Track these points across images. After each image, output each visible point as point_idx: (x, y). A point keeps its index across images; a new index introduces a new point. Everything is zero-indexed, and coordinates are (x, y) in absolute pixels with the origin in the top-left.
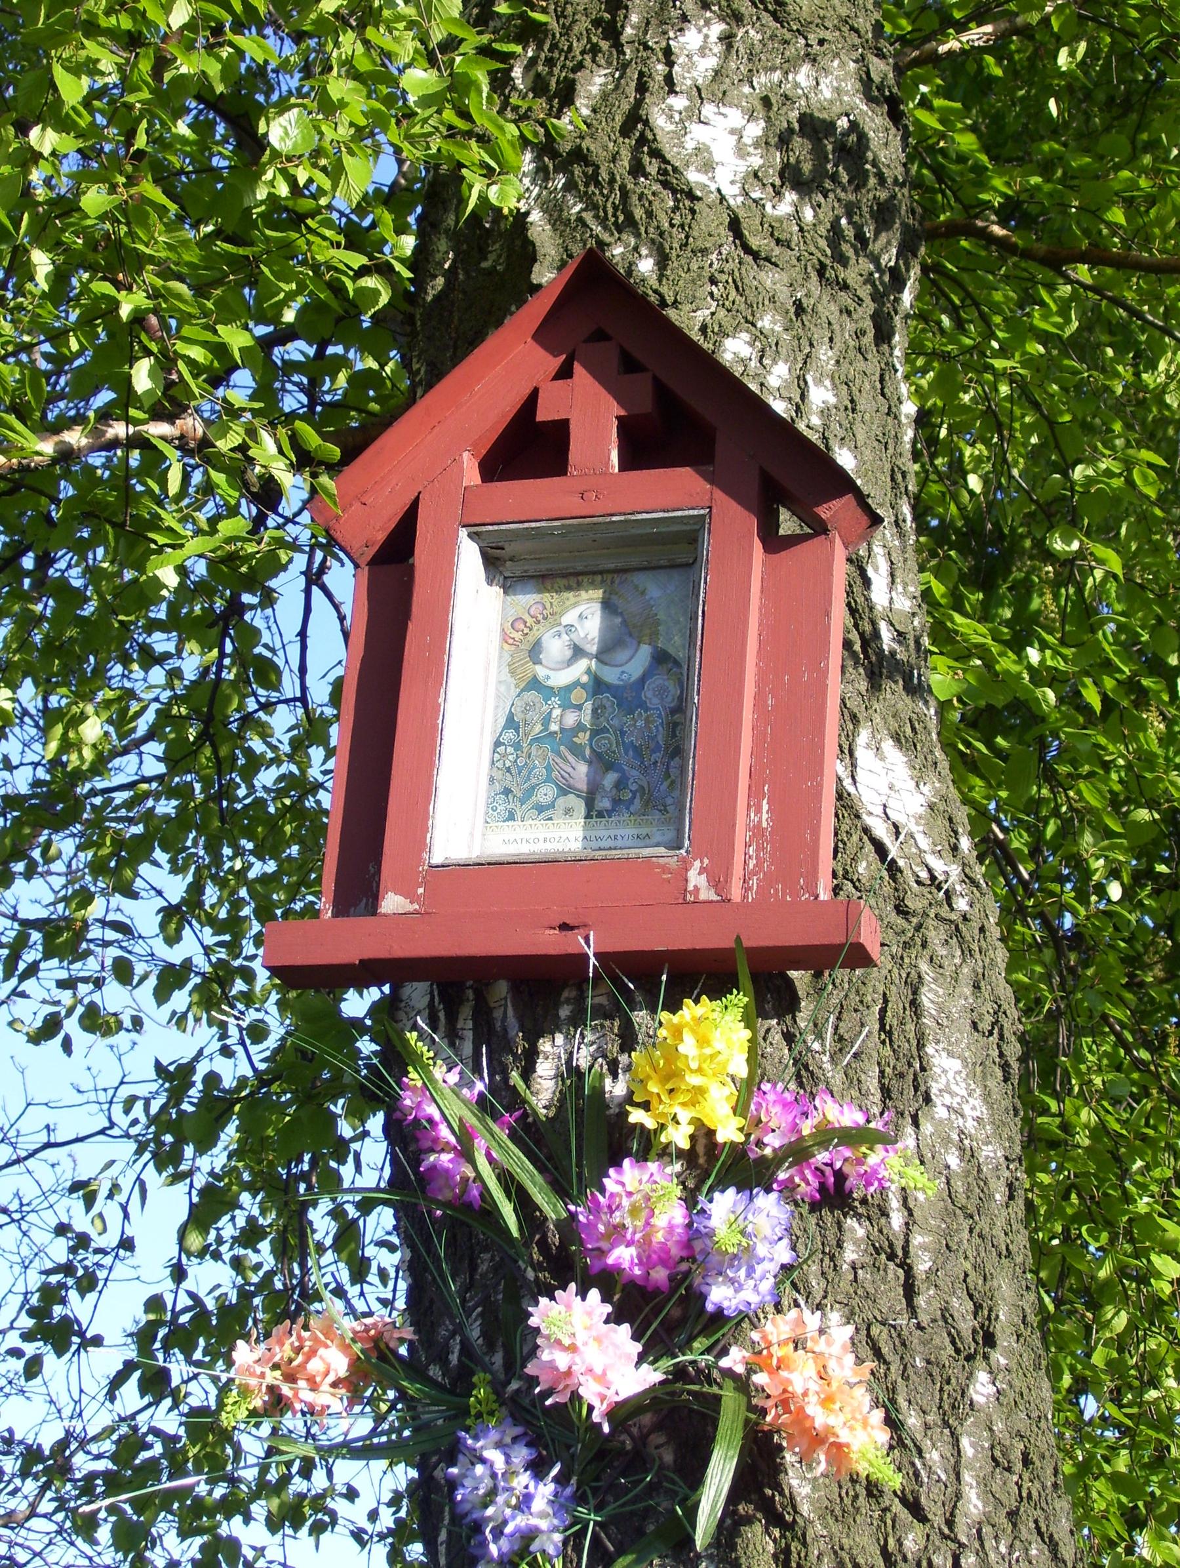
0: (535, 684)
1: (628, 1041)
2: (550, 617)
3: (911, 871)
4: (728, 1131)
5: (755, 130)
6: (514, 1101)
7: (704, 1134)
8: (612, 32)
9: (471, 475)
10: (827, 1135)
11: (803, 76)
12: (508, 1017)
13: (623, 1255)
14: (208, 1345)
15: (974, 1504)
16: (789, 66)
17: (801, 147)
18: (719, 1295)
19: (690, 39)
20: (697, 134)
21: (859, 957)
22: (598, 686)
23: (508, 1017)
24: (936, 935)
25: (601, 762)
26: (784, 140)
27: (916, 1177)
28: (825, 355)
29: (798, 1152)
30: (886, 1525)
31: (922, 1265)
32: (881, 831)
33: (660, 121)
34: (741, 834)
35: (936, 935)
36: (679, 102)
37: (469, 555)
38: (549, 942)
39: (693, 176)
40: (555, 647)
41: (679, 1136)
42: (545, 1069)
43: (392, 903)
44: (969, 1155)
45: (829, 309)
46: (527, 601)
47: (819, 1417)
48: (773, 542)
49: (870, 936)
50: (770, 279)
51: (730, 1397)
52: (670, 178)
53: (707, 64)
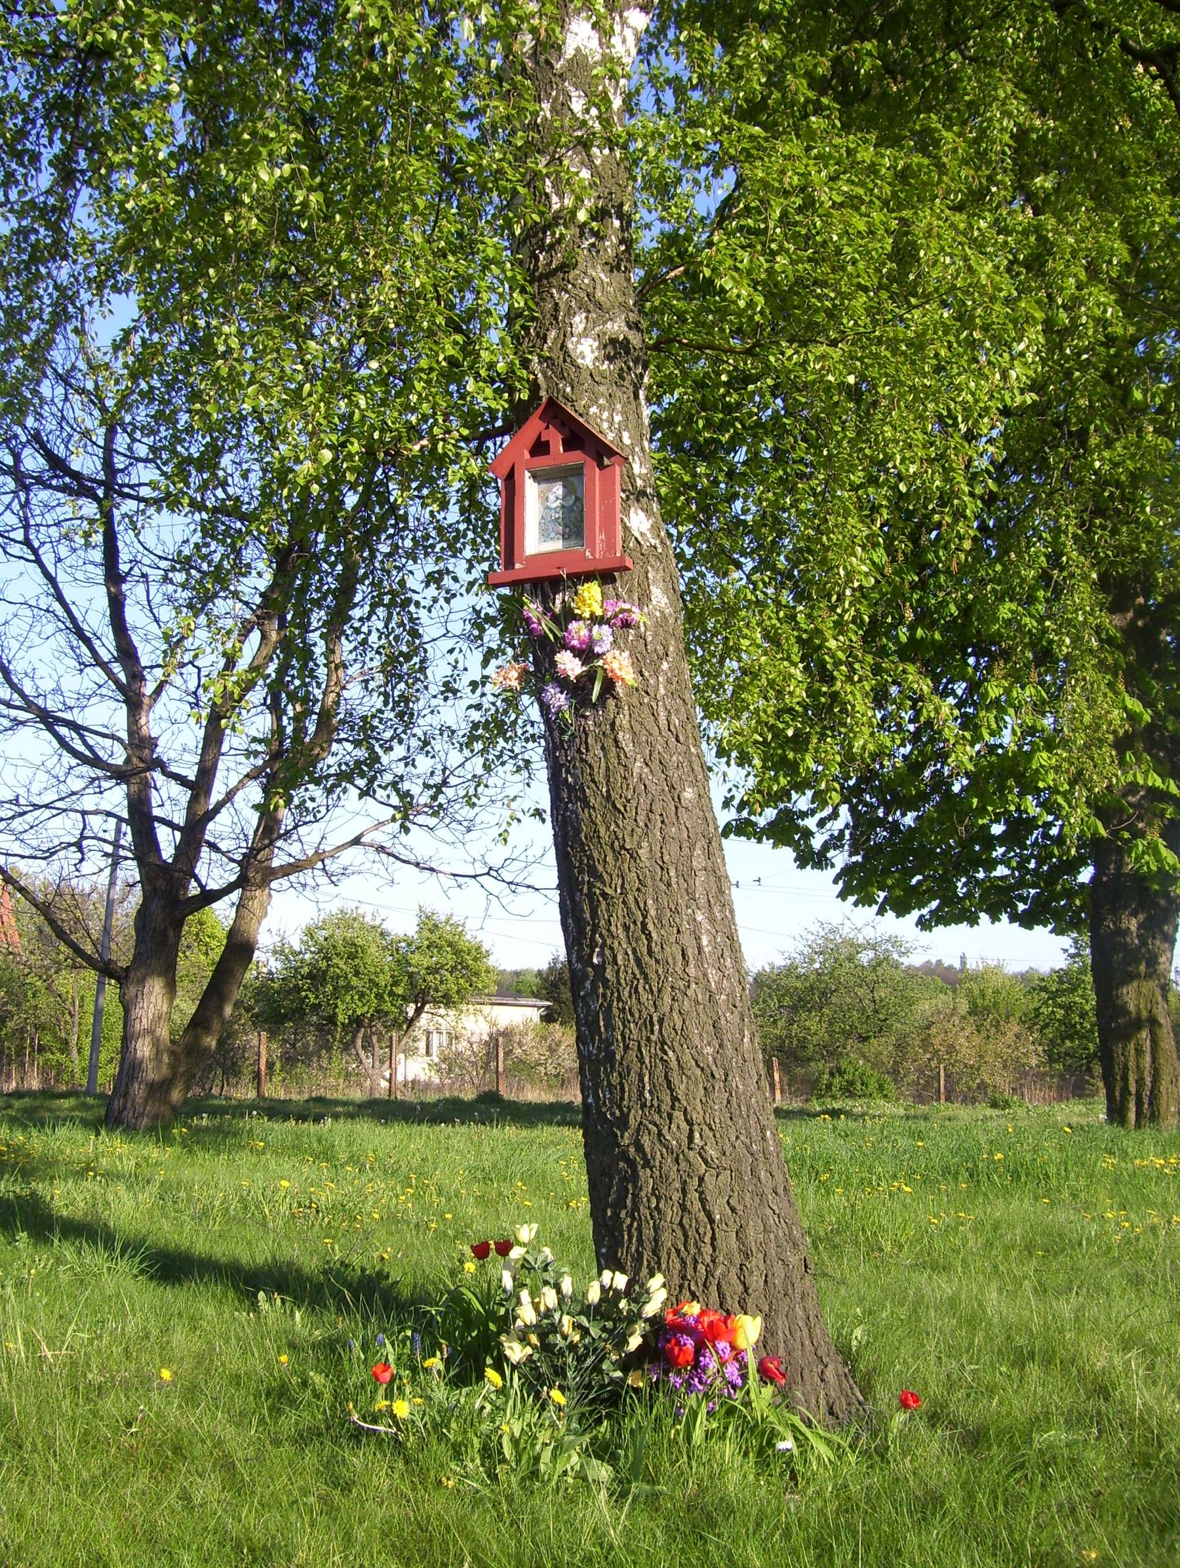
0: (548, 508)
1: (576, 593)
2: (550, 490)
3: (645, 545)
4: (599, 612)
5: (596, 344)
6: (550, 610)
7: (592, 614)
8: (556, 319)
9: (527, 455)
10: (622, 611)
11: (609, 325)
12: (548, 590)
13: (575, 643)
14: (938, 908)
15: (662, 691)
16: (604, 323)
17: (610, 349)
18: (597, 649)
19: (577, 319)
20: (580, 348)
21: (627, 569)
22: (563, 507)
23: (548, 590)
24: (652, 560)
25: (565, 526)
26: (605, 347)
27: (644, 619)
28: (619, 407)
29: (616, 616)
30: (640, 697)
31: (649, 639)
32: (637, 534)
33: (570, 346)
34: (598, 541)
35: (652, 560)
36: (575, 339)
37: (527, 474)
38: (555, 572)
39: (579, 361)
40: (552, 497)
41: (587, 615)
42: (558, 602)
43: (518, 566)
44: (662, 612)
45: (619, 394)
46: (544, 486)
47: (619, 673)
48: (601, 466)
49: (629, 563)
50: (602, 388)
51: (600, 672)
52: (573, 363)
53: (581, 327)
